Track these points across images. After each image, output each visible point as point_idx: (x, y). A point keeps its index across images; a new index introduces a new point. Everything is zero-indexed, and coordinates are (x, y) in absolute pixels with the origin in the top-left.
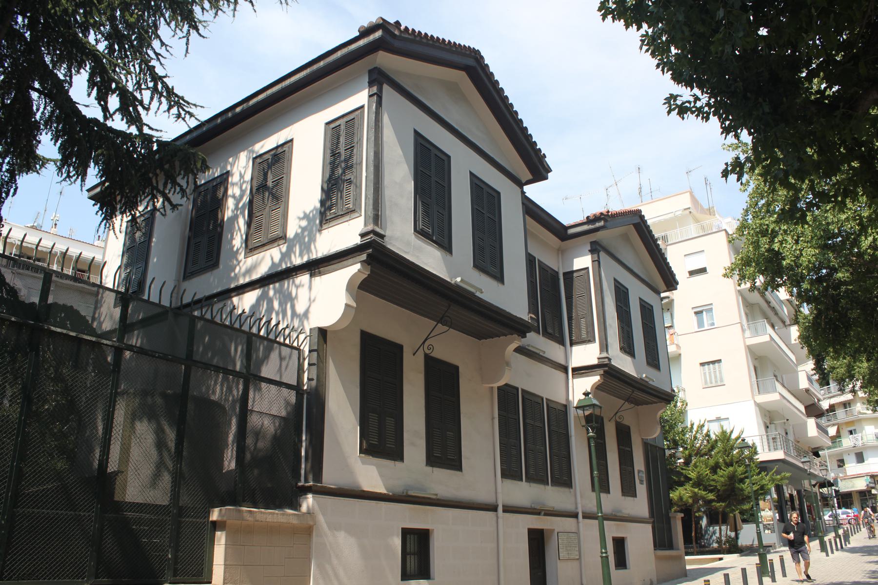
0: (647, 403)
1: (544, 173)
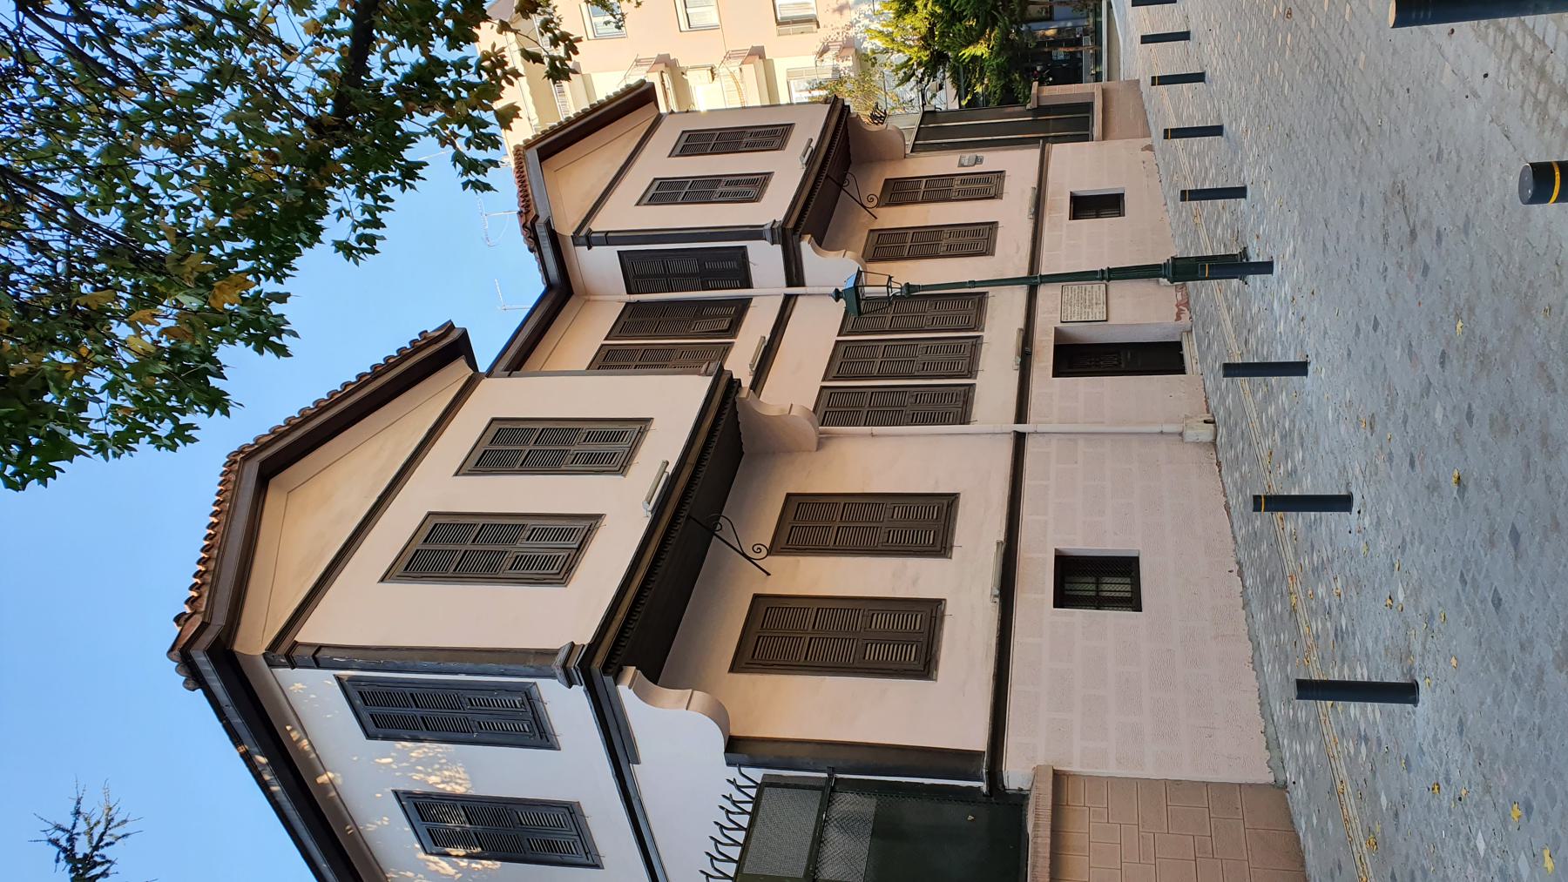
1: (454, 336)
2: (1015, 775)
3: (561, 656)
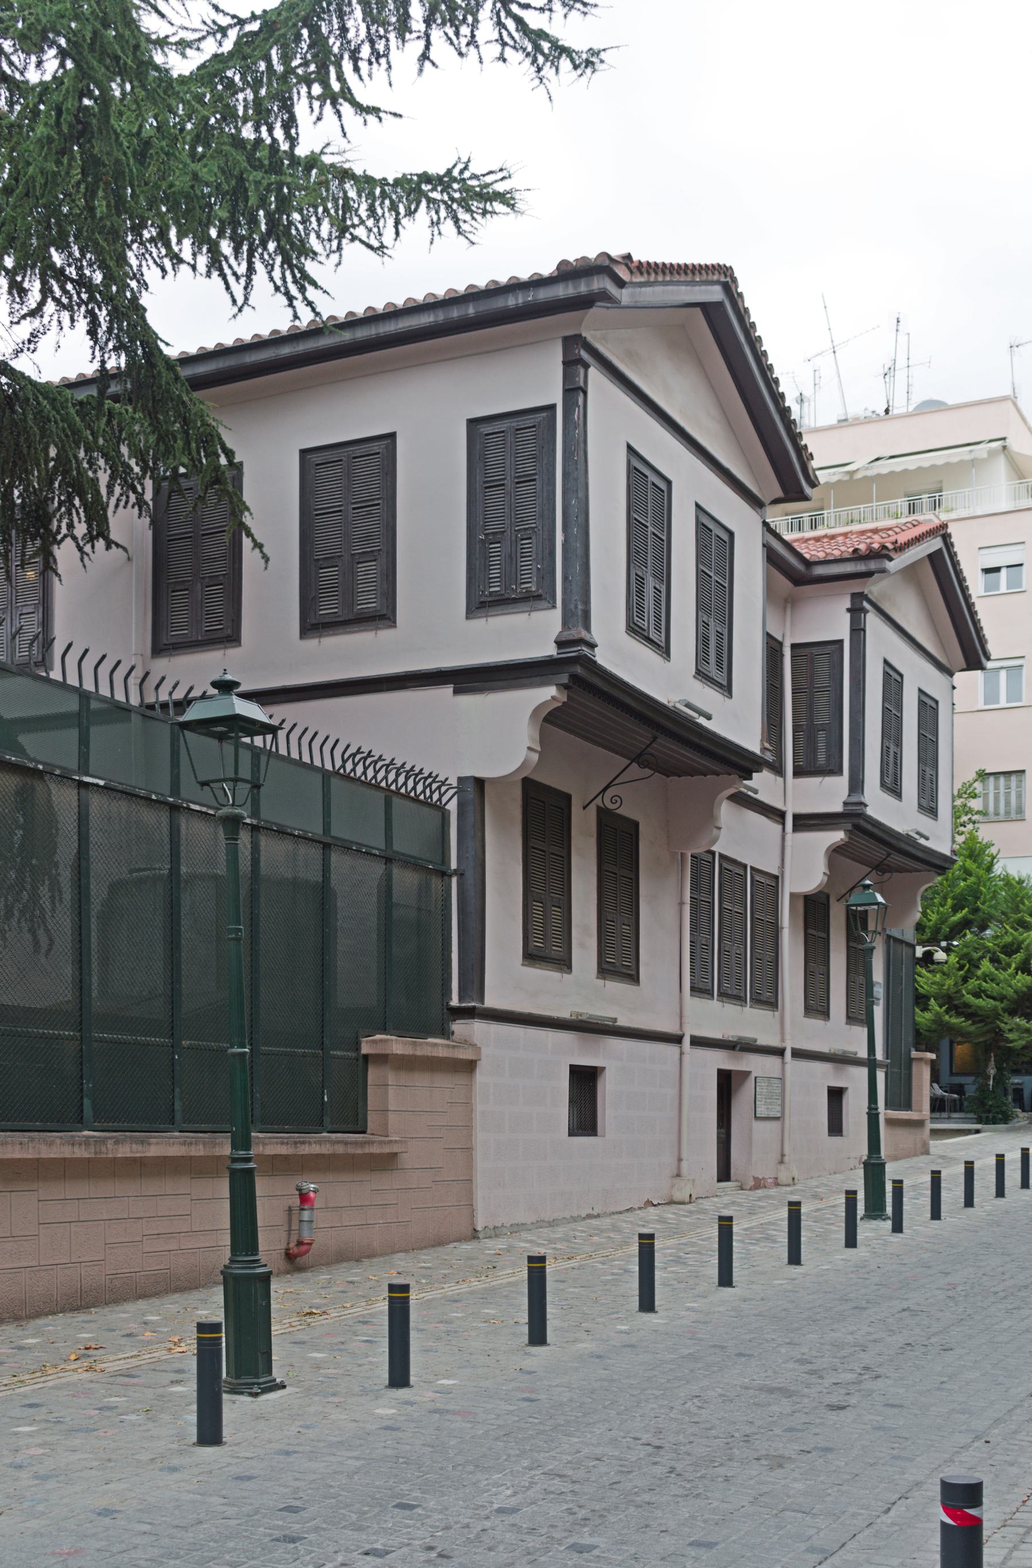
0: (692, 772)
1: (808, 490)
2: (478, 1030)
3: (584, 634)
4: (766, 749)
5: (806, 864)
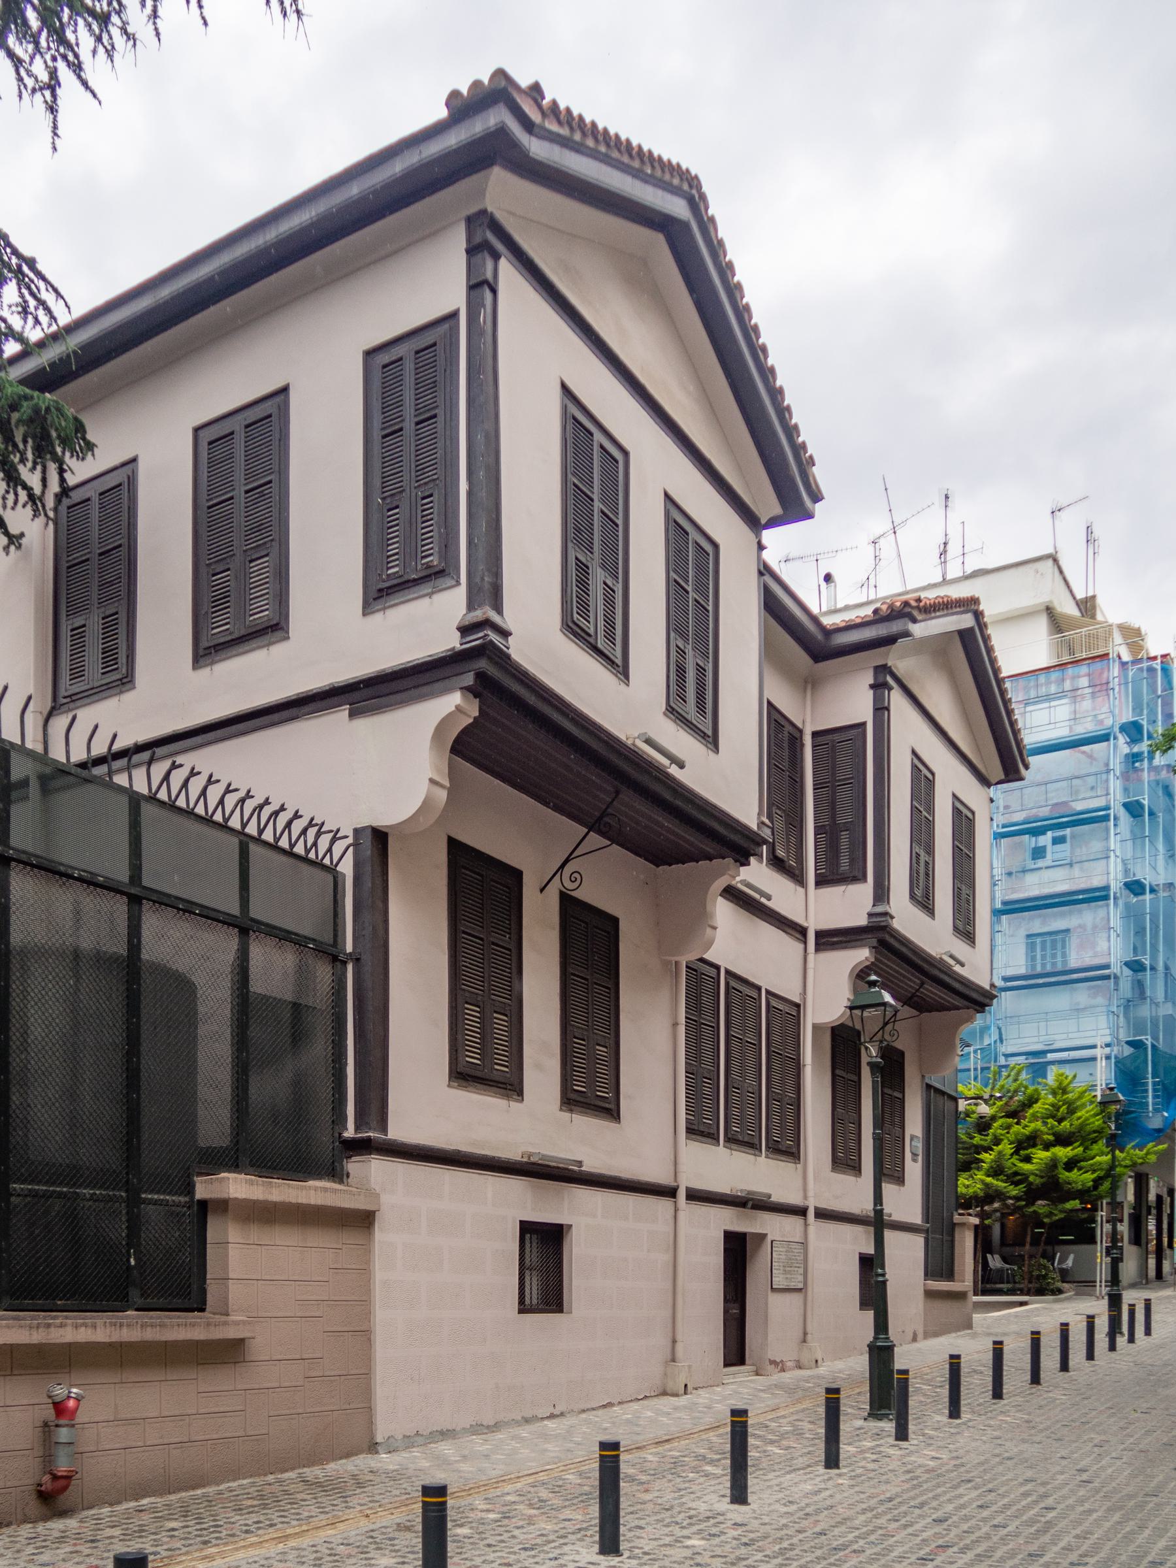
2: (374, 1172)
4: (763, 823)
5: (827, 991)
